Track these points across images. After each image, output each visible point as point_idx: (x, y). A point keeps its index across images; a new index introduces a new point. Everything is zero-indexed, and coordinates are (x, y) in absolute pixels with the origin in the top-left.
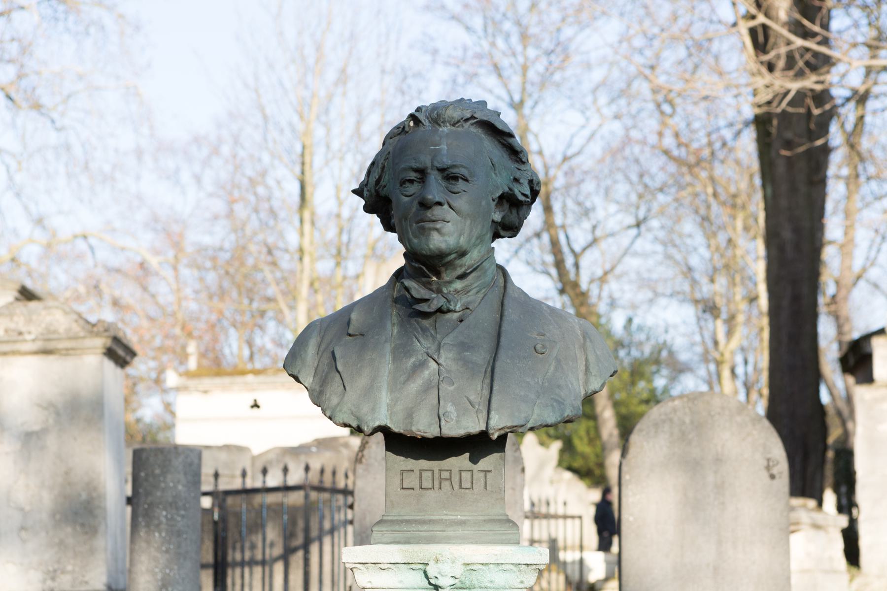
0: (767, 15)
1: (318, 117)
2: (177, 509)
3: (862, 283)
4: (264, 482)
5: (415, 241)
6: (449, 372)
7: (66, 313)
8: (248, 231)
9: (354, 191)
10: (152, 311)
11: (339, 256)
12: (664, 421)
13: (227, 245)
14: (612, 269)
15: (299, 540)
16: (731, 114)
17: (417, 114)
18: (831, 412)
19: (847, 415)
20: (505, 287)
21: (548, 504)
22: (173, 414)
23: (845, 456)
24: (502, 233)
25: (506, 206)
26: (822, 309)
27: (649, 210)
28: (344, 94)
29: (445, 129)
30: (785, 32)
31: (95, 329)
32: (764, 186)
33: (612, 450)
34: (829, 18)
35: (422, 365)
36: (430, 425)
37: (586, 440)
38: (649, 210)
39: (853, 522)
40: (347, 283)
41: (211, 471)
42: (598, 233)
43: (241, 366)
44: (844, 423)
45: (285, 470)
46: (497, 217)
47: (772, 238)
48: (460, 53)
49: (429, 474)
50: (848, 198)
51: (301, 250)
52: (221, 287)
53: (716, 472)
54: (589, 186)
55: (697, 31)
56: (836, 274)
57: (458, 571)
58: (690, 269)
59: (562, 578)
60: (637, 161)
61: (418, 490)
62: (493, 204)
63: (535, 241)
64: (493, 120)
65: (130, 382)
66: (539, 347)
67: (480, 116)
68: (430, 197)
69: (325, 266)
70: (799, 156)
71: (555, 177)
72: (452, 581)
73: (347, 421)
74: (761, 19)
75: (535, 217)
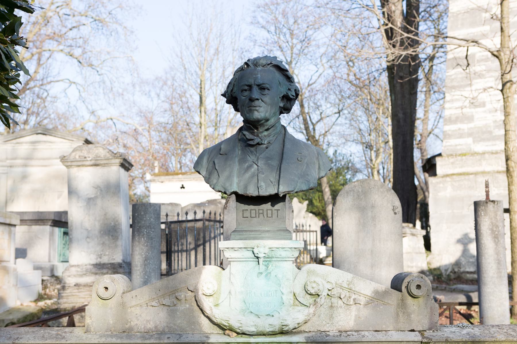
0: (392, 24)
1: (207, 68)
2: (151, 228)
3: (431, 135)
4: (187, 218)
5: (248, 115)
6: (262, 169)
7: (104, 149)
8: (179, 116)
9: (222, 95)
10: (140, 149)
11: (216, 126)
12: (351, 191)
13: (170, 122)
14: (329, 130)
15: (201, 242)
16: (377, 66)
17: (248, 62)
18: (419, 188)
19: (425, 189)
20: (285, 134)
21: (303, 226)
22: (149, 191)
23: (425, 206)
24: (284, 112)
25: (285, 100)
26: (415, 146)
27: (344, 106)
28: (218, 59)
29: (260, 68)
30: (400, 31)
31: (116, 156)
32: (391, 95)
33: (329, 204)
34: (418, 25)
35: (250, 166)
36: (254, 191)
37: (318, 200)
38: (344, 106)
39: (428, 233)
40: (219, 137)
41: (165, 214)
42: (323, 116)
43: (176, 171)
44: (424, 193)
45: (195, 213)
46: (282, 105)
47: (394, 117)
48: (265, 42)
49: (254, 211)
50: (426, 100)
51: (201, 123)
52: (168, 139)
53: (372, 212)
54: (319, 96)
55: (364, 31)
56: (421, 131)
57: (267, 251)
58: (360, 130)
59: (309, 256)
60: (339, 86)
61: (250, 218)
62: (280, 99)
63: (297, 119)
64: (279, 64)
65: (131, 178)
66: (299, 159)
67: (274, 63)
68: (254, 97)
69: (210, 130)
70: (405, 82)
71: (305, 93)
72: (264, 255)
73: (220, 190)
74: (390, 25)
75: (296, 108)
